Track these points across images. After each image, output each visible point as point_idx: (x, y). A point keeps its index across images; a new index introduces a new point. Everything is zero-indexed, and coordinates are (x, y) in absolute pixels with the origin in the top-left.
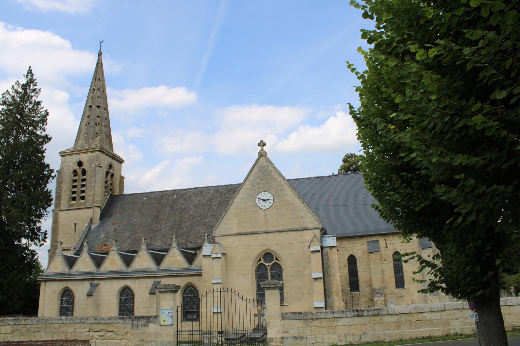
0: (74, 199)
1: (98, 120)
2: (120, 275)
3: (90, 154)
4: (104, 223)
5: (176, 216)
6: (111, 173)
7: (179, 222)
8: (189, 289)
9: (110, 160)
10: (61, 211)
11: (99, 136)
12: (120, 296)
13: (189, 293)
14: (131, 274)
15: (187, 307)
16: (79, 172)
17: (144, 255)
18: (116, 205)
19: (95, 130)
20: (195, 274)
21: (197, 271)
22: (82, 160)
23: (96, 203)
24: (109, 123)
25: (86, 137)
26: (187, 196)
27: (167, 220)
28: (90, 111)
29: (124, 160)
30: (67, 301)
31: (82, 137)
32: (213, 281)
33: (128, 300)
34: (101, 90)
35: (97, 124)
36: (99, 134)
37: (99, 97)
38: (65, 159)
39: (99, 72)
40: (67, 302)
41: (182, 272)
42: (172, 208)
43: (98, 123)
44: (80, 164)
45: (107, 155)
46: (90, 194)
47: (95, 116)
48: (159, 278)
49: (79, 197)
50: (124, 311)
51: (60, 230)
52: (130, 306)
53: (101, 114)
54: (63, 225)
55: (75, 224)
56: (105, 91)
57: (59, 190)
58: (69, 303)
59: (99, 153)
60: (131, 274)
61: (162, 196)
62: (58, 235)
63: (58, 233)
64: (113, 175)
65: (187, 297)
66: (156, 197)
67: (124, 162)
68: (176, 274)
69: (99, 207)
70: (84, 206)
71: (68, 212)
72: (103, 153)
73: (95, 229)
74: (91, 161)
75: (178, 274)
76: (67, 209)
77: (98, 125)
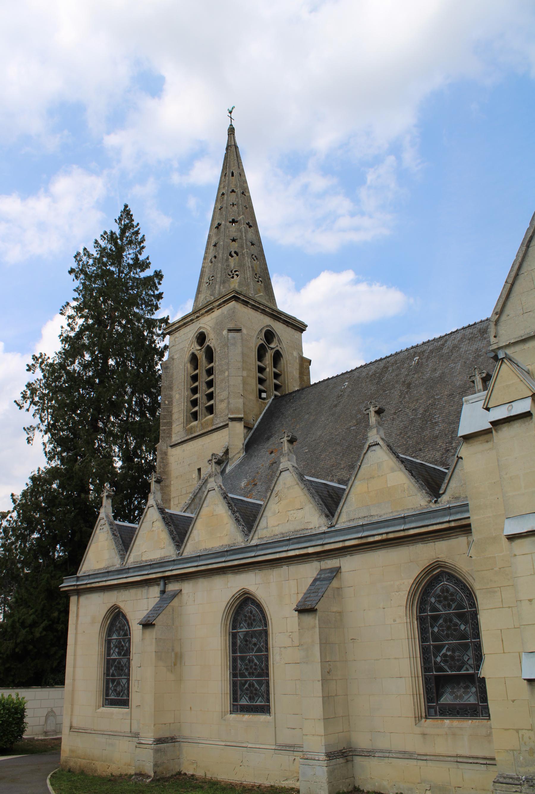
0: (195, 416)
1: (234, 246)
2: (223, 559)
3: (217, 313)
4: (251, 456)
5: (417, 400)
6: (274, 351)
7: (425, 411)
8: (438, 589)
9: (267, 321)
10: (172, 446)
11: (237, 275)
12: (234, 627)
13: (440, 602)
14: (253, 554)
15: (439, 659)
16: (202, 356)
17: (288, 488)
18: (283, 414)
19: (228, 266)
20: (453, 524)
21: (457, 513)
22: (203, 330)
23: (233, 413)
24: (262, 250)
25: (212, 283)
26: (445, 351)
27: (395, 413)
28: (217, 234)
29: (306, 323)
30: (119, 646)
31: (205, 286)
32: (512, 528)
33: (254, 640)
34: (239, 191)
35: (233, 254)
36: (237, 273)
37: (233, 205)
38: (176, 337)
39: (233, 157)
40: (119, 649)
41: (405, 523)
42: (409, 386)
43: (235, 253)
44: (201, 338)
45: (255, 308)
46: (222, 397)
47: (226, 240)
48: (336, 557)
49: (204, 409)
50: (246, 677)
51: (173, 488)
52: (259, 658)
53: (239, 233)
54: (177, 478)
55: (199, 470)
56: (247, 194)
57: (167, 402)
58: (123, 650)
59: (233, 303)
60: (253, 554)
61: (384, 367)
62: (170, 500)
63: (170, 495)
64: (277, 357)
65: (435, 618)
66: (370, 373)
67: (307, 328)
68: (384, 537)
69: (240, 419)
70: (213, 425)
71: (184, 446)
72: (246, 303)
73: (233, 471)
74: (219, 326)
75: (391, 536)
76: (183, 440)
77: (234, 255)
